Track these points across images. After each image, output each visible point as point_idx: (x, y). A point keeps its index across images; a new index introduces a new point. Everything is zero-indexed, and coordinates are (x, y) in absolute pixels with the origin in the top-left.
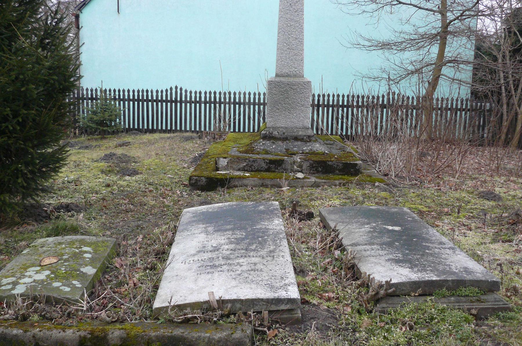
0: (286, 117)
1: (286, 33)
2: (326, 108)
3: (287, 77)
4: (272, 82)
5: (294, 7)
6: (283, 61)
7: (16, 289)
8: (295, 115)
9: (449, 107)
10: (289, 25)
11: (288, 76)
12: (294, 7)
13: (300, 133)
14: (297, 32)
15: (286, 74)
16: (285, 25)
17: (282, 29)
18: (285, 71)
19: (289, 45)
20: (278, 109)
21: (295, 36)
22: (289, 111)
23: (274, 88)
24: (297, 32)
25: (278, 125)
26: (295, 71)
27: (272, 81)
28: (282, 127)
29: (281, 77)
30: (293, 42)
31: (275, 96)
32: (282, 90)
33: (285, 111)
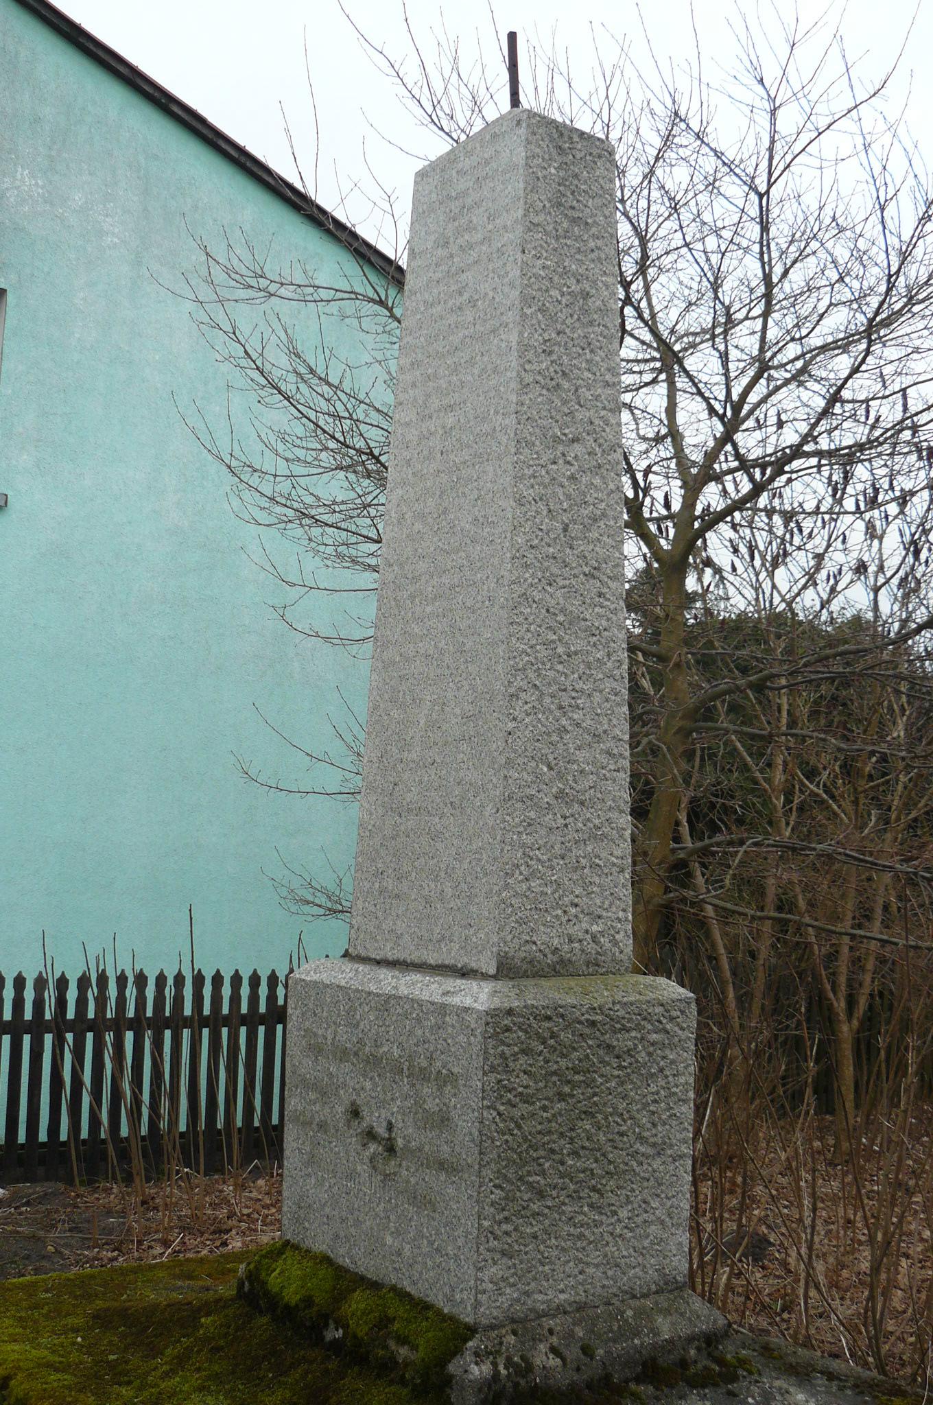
0: (581, 1237)
1: (548, 700)
2: (206, 1032)
3: (557, 974)
4: (507, 1021)
5: (581, 546)
6: (533, 874)
7: (145, 972)
8: (623, 1214)
9: (131, 1013)
10: (560, 650)
11: (560, 968)
12: (581, 546)
13: (666, 1328)
14: (597, 698)
15: (551, 959)
16: (543, 652)
17: (532, 675)
18: (549, 937)
19: (561, 777)
20: (541, 1195)
21: (587, 723)
22: (595, 1196)
23: (523, 1059)
24: (597, 698)
25: (539, 1301)
26: (594, 939)
27: (510, 1012)
28: (561, 1310)
29: (525, 975)
30: (581, 755)
31: (524, 1109)
32: (563, 1063)
33: (575, 1197)
